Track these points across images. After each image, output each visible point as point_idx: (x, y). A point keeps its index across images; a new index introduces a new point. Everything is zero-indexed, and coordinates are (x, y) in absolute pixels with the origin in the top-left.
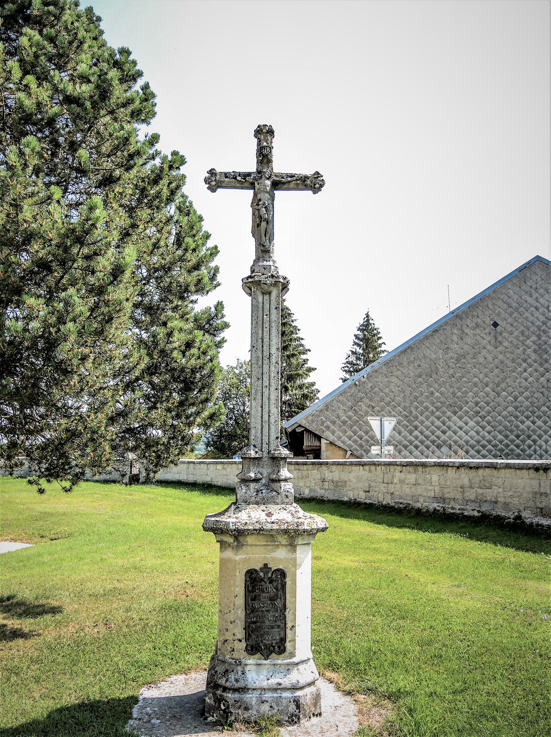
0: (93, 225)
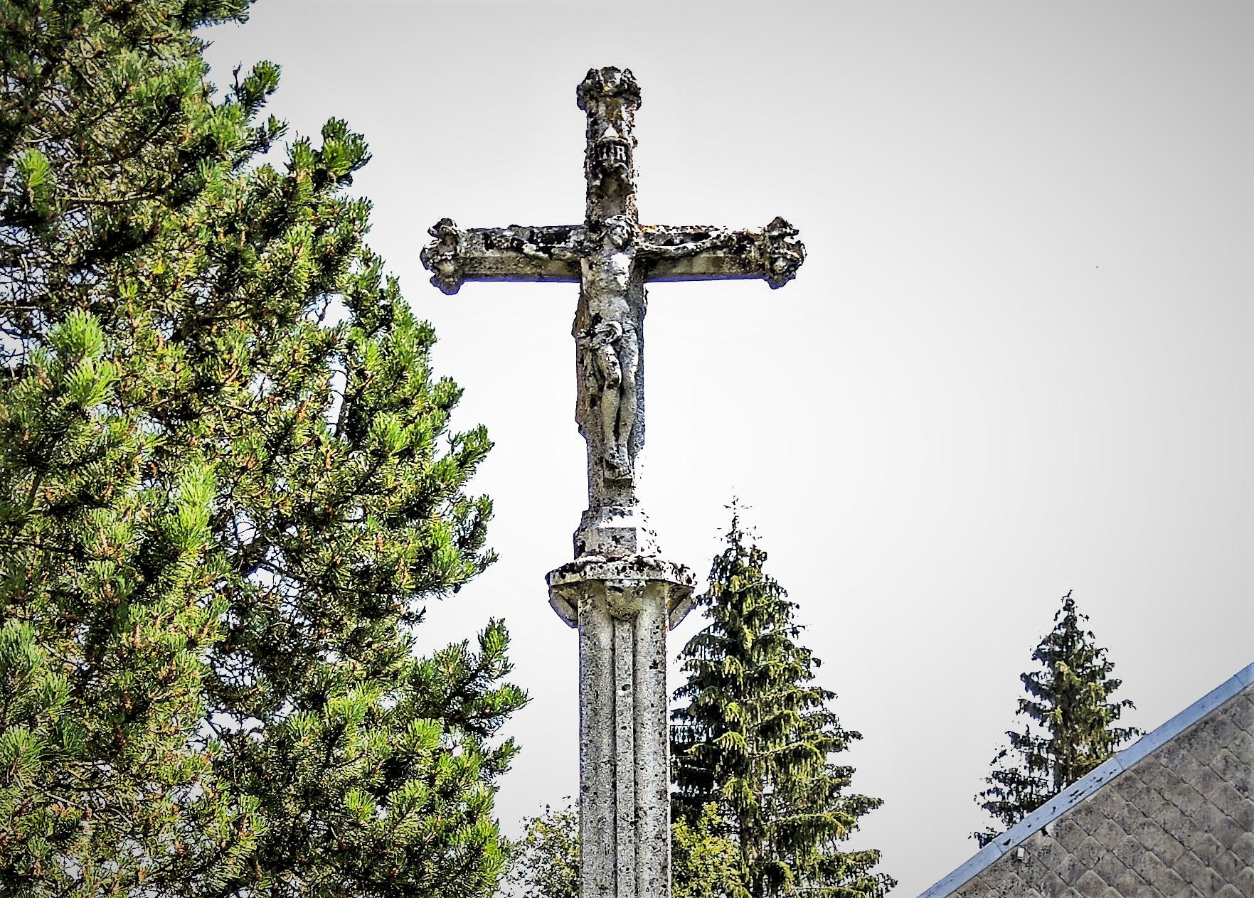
0: (76, 408)
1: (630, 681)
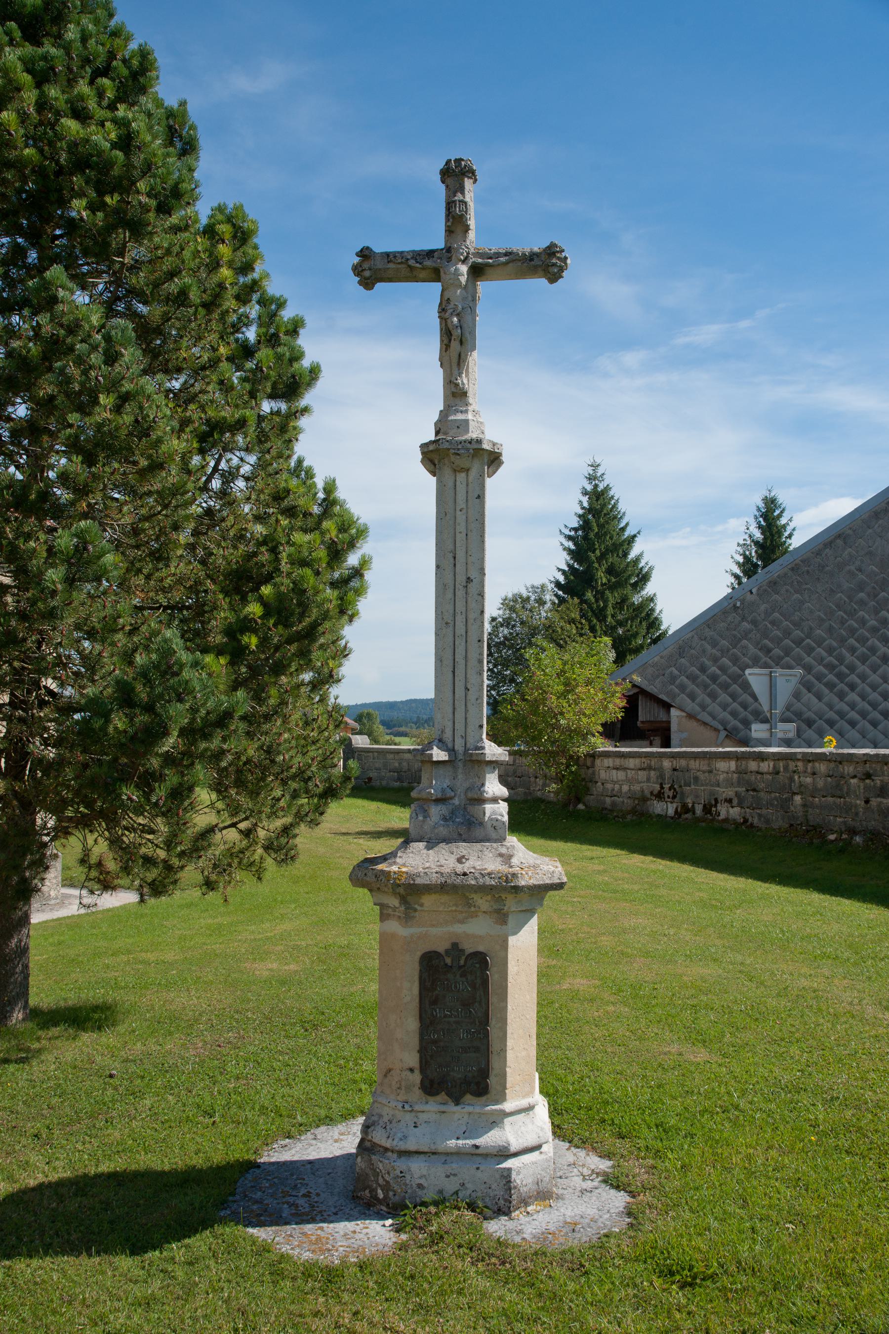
1: (464, 506)
